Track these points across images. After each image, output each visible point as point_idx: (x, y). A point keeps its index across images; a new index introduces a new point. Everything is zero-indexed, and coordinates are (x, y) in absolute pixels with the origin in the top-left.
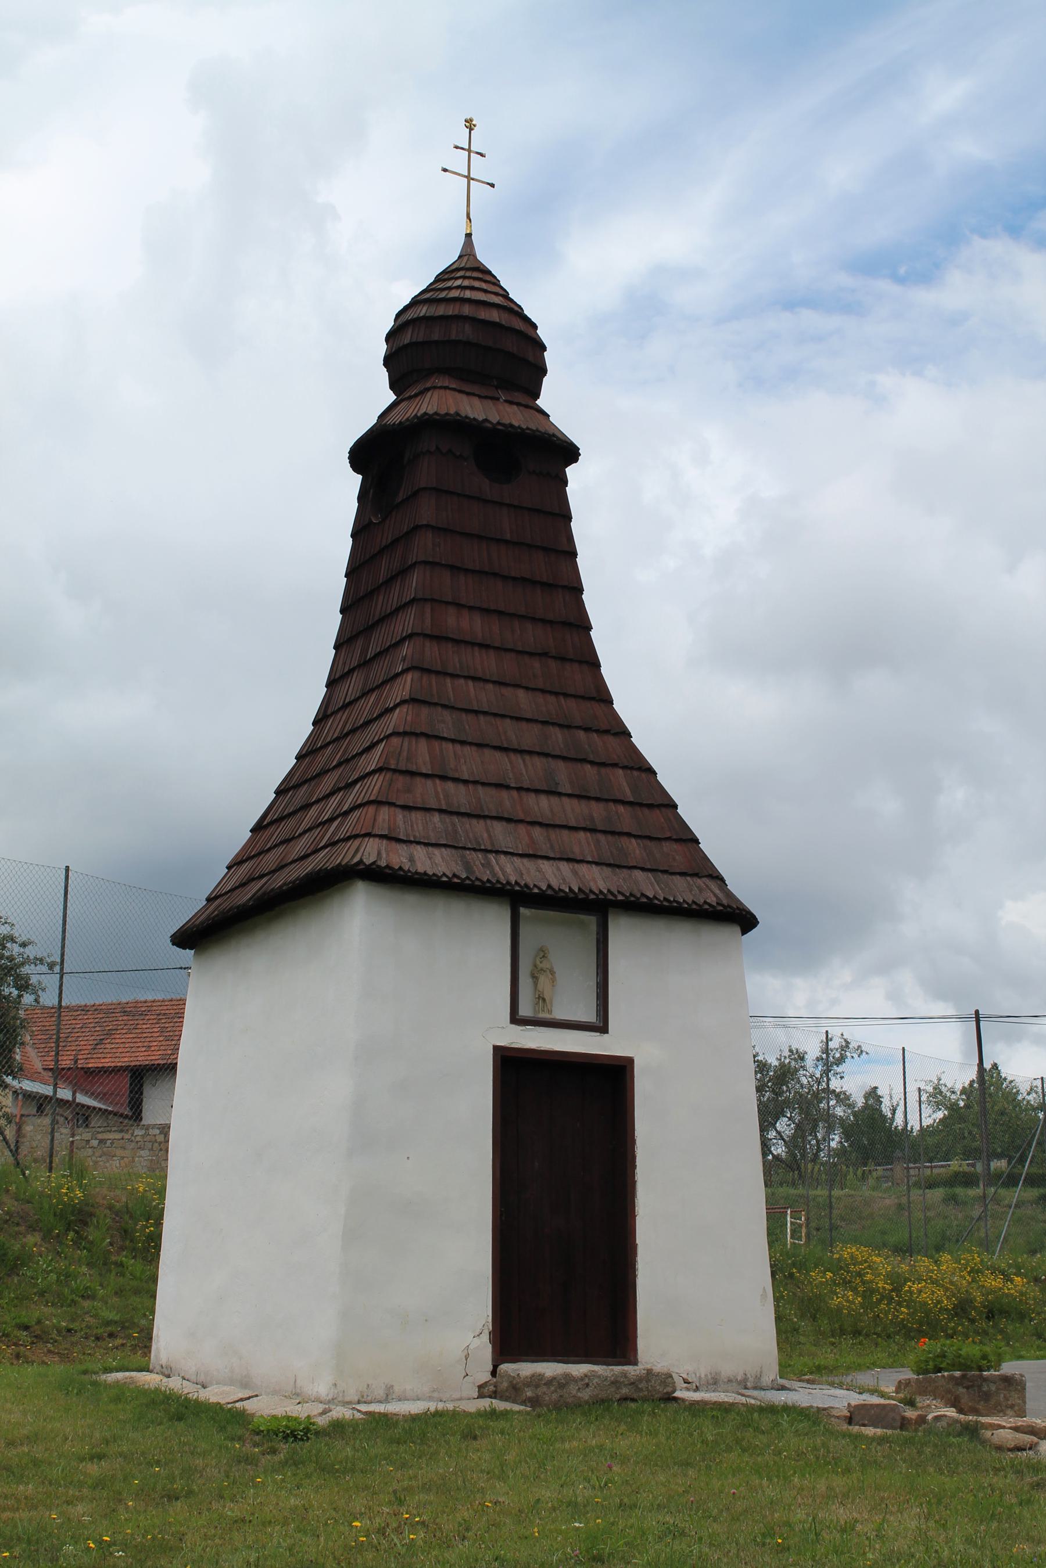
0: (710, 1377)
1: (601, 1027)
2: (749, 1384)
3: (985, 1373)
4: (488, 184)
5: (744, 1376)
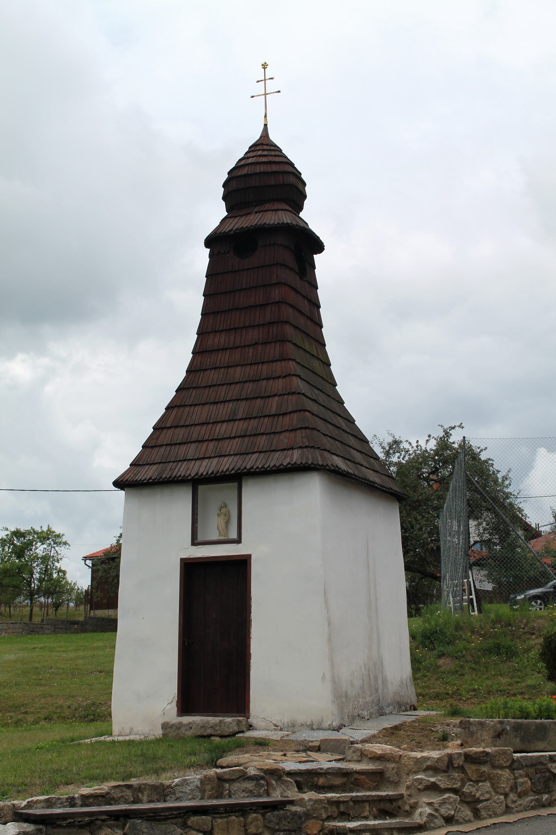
0: (290, 723)
1: (238, 541)
2: (314, 727)
3: (472, 720)
4: (276, 92)
5: (311, 723)
